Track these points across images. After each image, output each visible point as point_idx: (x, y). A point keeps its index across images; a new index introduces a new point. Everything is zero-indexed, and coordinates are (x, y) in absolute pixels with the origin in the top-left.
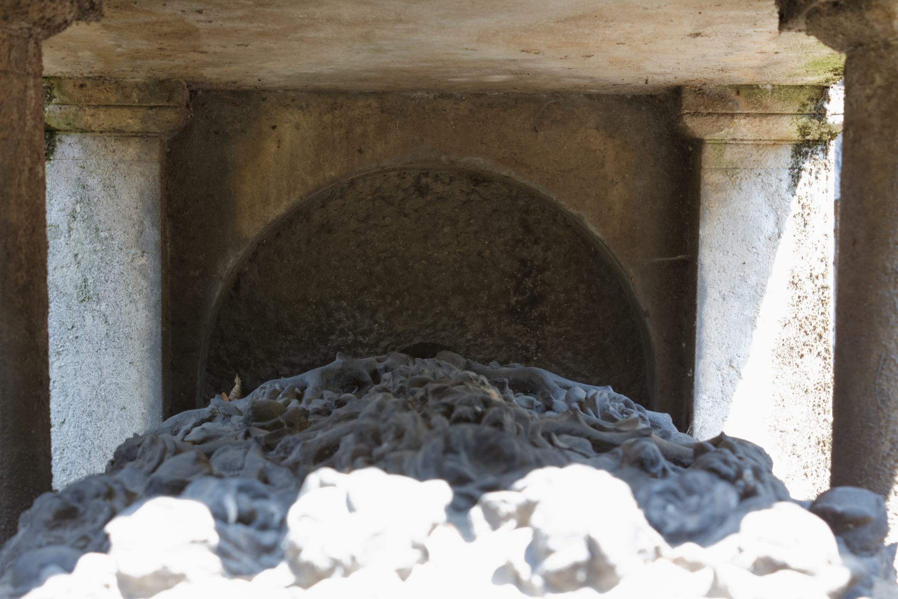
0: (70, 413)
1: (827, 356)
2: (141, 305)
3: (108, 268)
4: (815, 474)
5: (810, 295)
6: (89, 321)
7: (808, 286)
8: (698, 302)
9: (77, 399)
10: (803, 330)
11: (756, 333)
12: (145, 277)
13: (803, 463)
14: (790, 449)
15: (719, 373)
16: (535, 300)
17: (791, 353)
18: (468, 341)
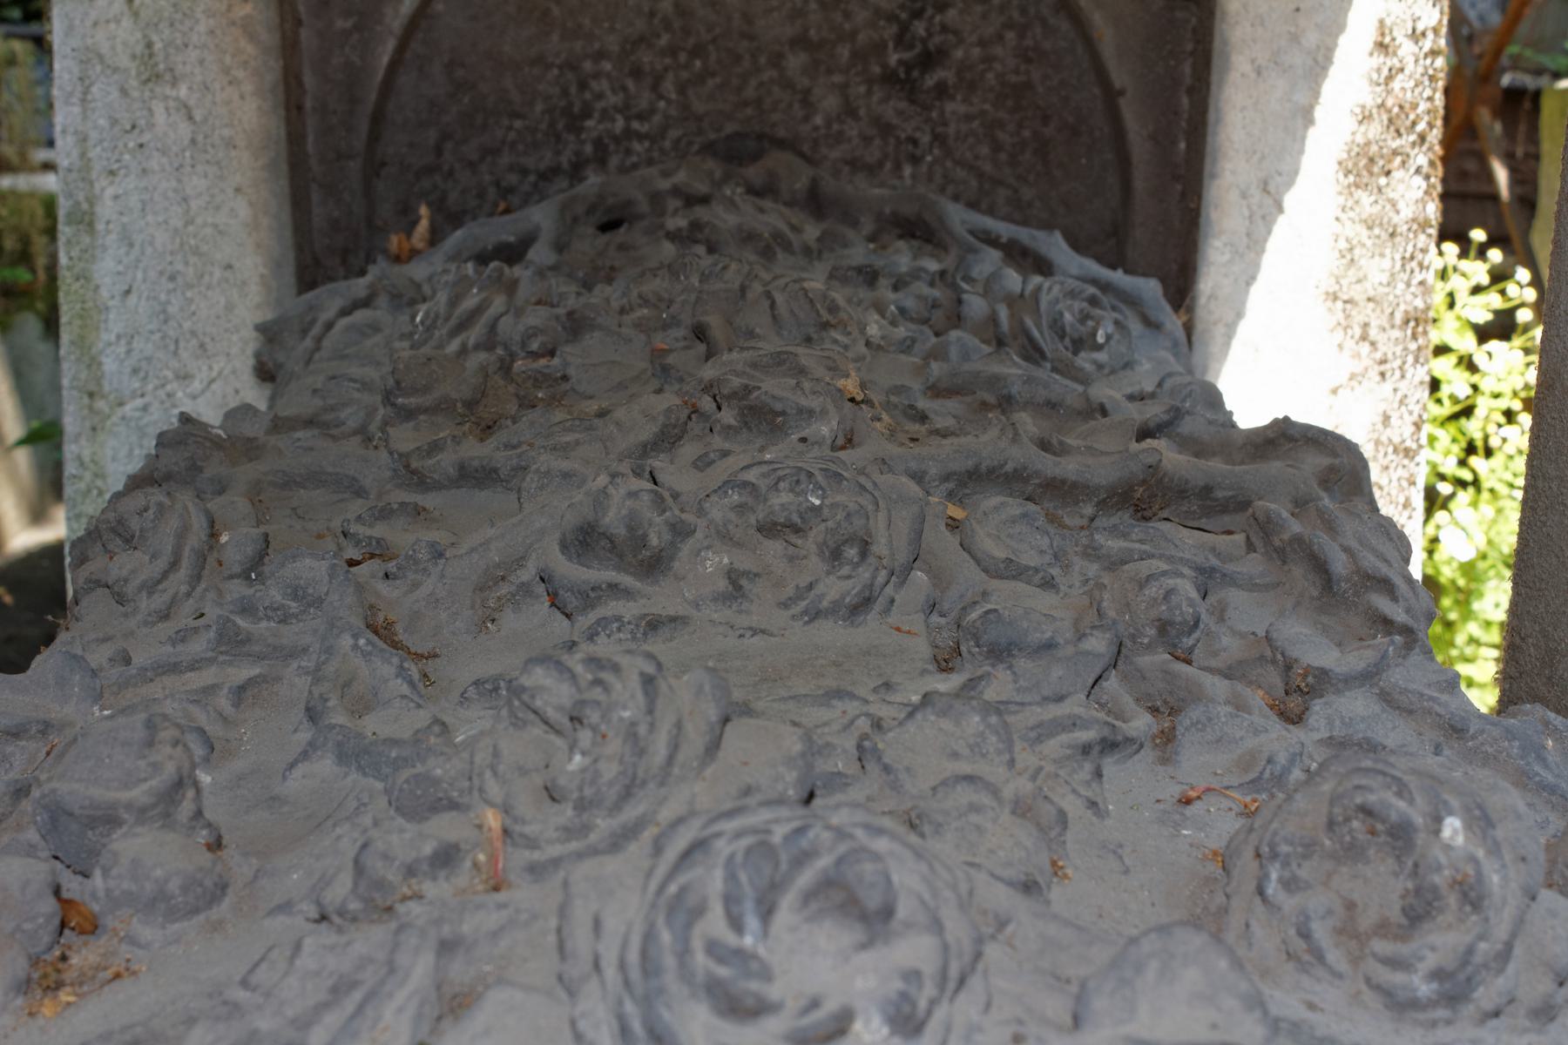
0: (140, 275)
1: (1432, 172)
2: (248, 88)
3: (188, 23)
4: (1398, 373)
5: (1410, 68)
6: (160, 117)
7: (1407, 49)
8: (1214, 78)
9: (149, 250)
10: (1392, 129)
11: (1312, 133)
12: (252, 37)
13: (1378, 355)
14: (1358, 332)
15: (1244, 202)
16: (929, 60)
17: (1366, 167)
18: (816, 128)
